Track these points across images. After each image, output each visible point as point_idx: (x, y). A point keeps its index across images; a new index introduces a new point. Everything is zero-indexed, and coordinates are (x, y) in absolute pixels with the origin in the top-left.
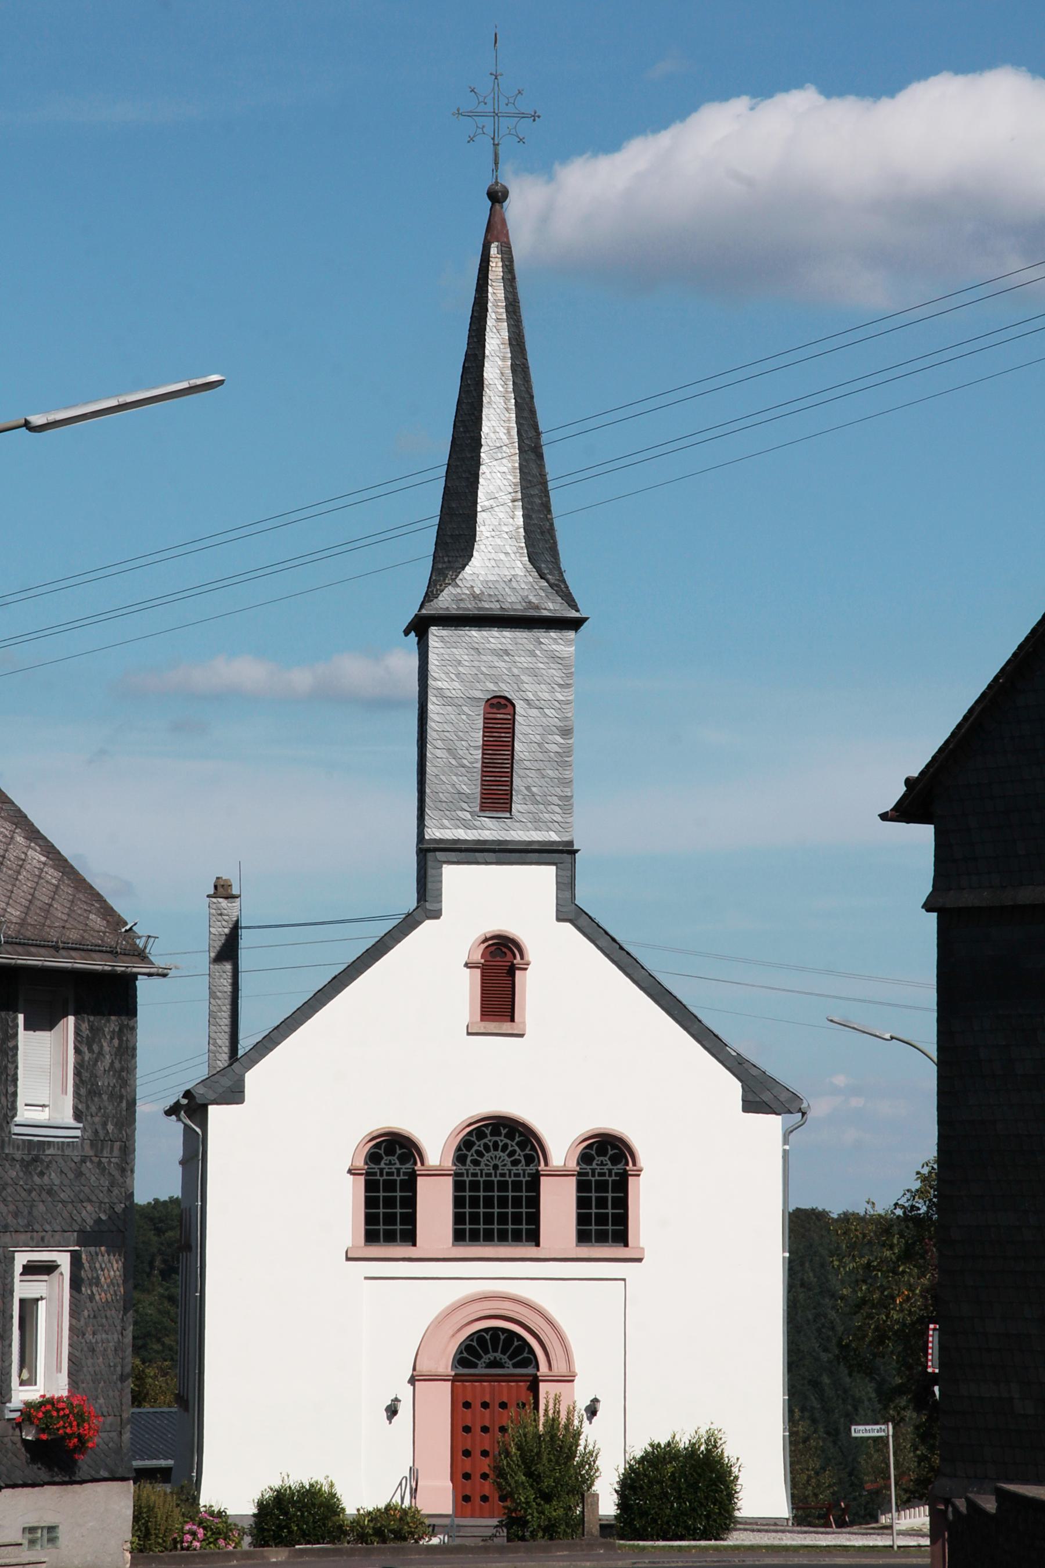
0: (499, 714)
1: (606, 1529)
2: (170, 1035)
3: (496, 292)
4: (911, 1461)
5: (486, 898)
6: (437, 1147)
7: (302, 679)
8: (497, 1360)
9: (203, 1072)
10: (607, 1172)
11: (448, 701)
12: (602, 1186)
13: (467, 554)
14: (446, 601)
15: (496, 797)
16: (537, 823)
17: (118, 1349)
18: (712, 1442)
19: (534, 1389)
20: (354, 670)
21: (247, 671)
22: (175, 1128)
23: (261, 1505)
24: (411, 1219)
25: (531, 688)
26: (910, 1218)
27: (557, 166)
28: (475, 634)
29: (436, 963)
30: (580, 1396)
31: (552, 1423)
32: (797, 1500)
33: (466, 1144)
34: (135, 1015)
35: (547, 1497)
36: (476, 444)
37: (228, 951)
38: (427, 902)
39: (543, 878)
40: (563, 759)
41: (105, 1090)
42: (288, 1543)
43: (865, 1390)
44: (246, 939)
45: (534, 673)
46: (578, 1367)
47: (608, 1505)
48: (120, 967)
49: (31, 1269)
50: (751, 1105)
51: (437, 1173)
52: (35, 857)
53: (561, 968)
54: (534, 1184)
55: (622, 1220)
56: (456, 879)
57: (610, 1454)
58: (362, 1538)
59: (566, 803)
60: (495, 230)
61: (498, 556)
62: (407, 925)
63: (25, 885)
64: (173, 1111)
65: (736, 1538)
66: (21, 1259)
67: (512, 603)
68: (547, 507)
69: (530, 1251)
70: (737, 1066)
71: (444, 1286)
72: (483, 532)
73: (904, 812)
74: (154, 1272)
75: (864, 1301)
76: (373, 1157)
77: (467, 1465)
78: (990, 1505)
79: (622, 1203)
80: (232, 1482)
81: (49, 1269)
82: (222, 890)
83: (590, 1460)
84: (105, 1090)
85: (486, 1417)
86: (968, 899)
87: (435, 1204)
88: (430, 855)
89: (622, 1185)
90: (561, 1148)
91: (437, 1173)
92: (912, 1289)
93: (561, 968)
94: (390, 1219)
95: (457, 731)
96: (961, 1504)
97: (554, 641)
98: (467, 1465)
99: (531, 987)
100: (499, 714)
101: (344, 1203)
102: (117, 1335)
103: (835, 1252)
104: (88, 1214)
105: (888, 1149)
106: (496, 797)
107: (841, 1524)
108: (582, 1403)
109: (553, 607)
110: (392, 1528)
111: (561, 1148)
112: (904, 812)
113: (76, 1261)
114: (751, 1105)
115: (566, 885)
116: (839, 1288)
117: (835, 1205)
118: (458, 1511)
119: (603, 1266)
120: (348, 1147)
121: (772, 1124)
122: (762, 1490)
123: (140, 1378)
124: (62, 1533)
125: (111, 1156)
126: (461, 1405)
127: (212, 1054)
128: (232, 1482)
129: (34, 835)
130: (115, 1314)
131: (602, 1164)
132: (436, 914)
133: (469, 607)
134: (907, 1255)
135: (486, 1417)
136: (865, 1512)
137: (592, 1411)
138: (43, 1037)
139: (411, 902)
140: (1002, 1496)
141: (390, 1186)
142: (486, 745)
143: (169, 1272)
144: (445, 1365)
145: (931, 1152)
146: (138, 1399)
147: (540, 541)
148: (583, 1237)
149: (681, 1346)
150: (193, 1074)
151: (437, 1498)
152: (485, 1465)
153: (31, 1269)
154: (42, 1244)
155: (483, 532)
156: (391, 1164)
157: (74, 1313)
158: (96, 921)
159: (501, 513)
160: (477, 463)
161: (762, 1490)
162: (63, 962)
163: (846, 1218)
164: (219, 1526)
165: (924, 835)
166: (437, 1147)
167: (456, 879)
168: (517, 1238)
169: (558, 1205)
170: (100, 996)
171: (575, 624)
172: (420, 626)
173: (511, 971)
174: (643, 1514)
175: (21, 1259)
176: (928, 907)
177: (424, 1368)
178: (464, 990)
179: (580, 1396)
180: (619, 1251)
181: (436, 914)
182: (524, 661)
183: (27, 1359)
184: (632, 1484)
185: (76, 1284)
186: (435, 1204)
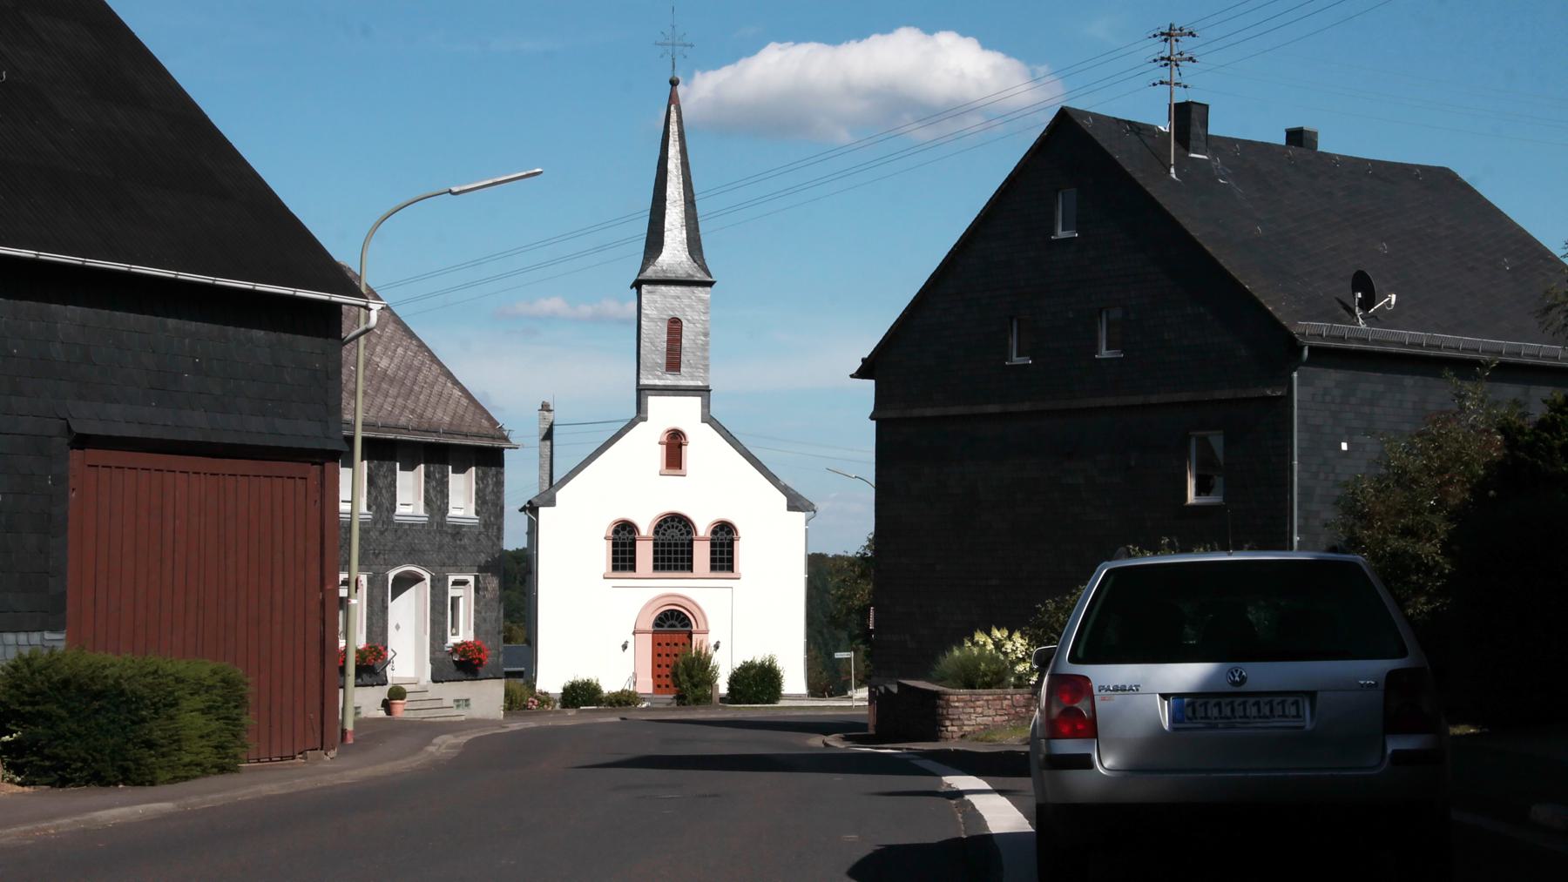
0: (675, 326)
1: (723, 699)
2: (520, 478)
3: (673, 128)
4: (862, 667)
5: (667, 412)
6: (645, 527)
7: (586, 310)
8: (673, 624)
9: (537, 492)
10: (724, 541)
11: (652, 320)
12: (722, 545)
13: (659, 251)
14: (650, 273)
15: (673, 364)
16: (693, 377)
17: (497, 620)
18: (771, 661)
19: (690, 637)
20: (611, 307)
21: (553, 304)
22: (524, 517)
23: (565, 689)
24: (633, 560)
25: (690, 314)
26: (863, 558)
27: (698, 75)
28: (663, 288)
29: (645, 442)
30: (711, 640)
31: (698, 653)
32: (810, 685)
33: (659, 526)
34: (502, 465)
35: (695, 686)
36: (664, 199)
37: (549, 435)
38: (641, 414)
39: (695, 402)
40: (705, 347)
41: (490, 502)
42: (577, 706)
43: (844, 635)
44: (556, 430)
45: (690, 306)
46: (711, 627)
47: (723, 687)
48: (496, 444)
49: (456, 583)
50: (791, 508)
51: (645, 539)
52: (457, 393)
53: (703, 444)
54: (691, 544)
55: (731, 560)
56: (653, 402)
57: (724, 668)
58: (611, 704)
59: (706, 368)
60: (673, 99)
61: (674, 253)
62: (631, 425)
63: (452, 404)
64: (523, 509)
65: (782, 703)
66: (451, 579)
67: (681, 274)
68: (697, 229)
69: (688, 574)
70: (785, 490)
71: (650, 590)
72: (666, 242)
73: (862, 373)
74: (513, 582)
75: (842, 596)
76: (616, 532)
77: (659, 671)
78: (895, 689)
79: (731, 553)
80: (551, 679)
81: (464, 583)
82: (545, 407)
83: (715, 668)
84: (490, 502)
85: (667, 650)
86: (890, 414)
87: (645, 553)
88: (642, 392)
89: (731, 544)
90: (703, 528)
91: (645, 539)
92: (864, 590)
93: (703, 444)
94: (624, 560)
95: (656, 335)
96: (882, 689)
97: (700, 292)
98: (659, 671)
99: (690, 453)
100: (675, 326)
101: (603, 553)
102: (496, 614)
103: (830, 573)
104: (482, 558)
105: (853, 528)
106: (673, 364)
107: (831, 696)
108: (713, 643)
109: (700, 276)
110: (624, 700)
111: (703, 528)
112: (862, 373)
113: (477, 579)
114: (791, 508)
115: (706, 406)
116: (831, 591)
117: (830, 551)
118: (655, 691)
119: (721, 582)
120: (604, 527)
121: (800, 517)
122: (794, 682)
123: (509, 630)
124: (472, 702)
125: (493, 532)
126: (656, 644)
127: (541, 484)
128: (551, 679)
129: (456, 383)
130: (495, 604)
131: (722, 535)
132: (645, 419)
133: (661, 276)
134: (863, 575)
135: (667, 650)
136: (841, 690)
137: (717, 647)
138: (409, 474)
139: (633, 413)
140: (900, 686)
141: (624, 545)
142: (669, 341)
143: (523, 582)
144: (649, 626)
145: (873, 530)
146: (507, 640)
147: (694, 245)
148: (713, 568)
149: (758, 619)
150: (532, 493)
151: (645, 686)
152: (668, 671)
153: (456, 583)
154: (461, 572)
155: (666, 242)
156: (624, 535)
157: (476, 603)
158: (485, 423)
159: (676, 232)
160: (664, 208)
161: (794, 682)
162: (419, 438)
163: (837, 558)
164: (545, 699)
165: (870, 384)
166: (645, 527)
167: (653, 402)
168: (682, 568)
169: (702, 554)
170: (487, 458)
171: (710, 284)
172: (638, 285)
173: (680, 446)
174: (740, 692)
175: (451, 579)
176: (872, 418)
177: (639, 627)
178: (659, 454)
179: (711, 640)
180: (729, 574)
181: (645, 419)
182: (686, 301)
183: (455, 624)
184: (735, 680)
185: (477, 590)
186: (645, 553)
